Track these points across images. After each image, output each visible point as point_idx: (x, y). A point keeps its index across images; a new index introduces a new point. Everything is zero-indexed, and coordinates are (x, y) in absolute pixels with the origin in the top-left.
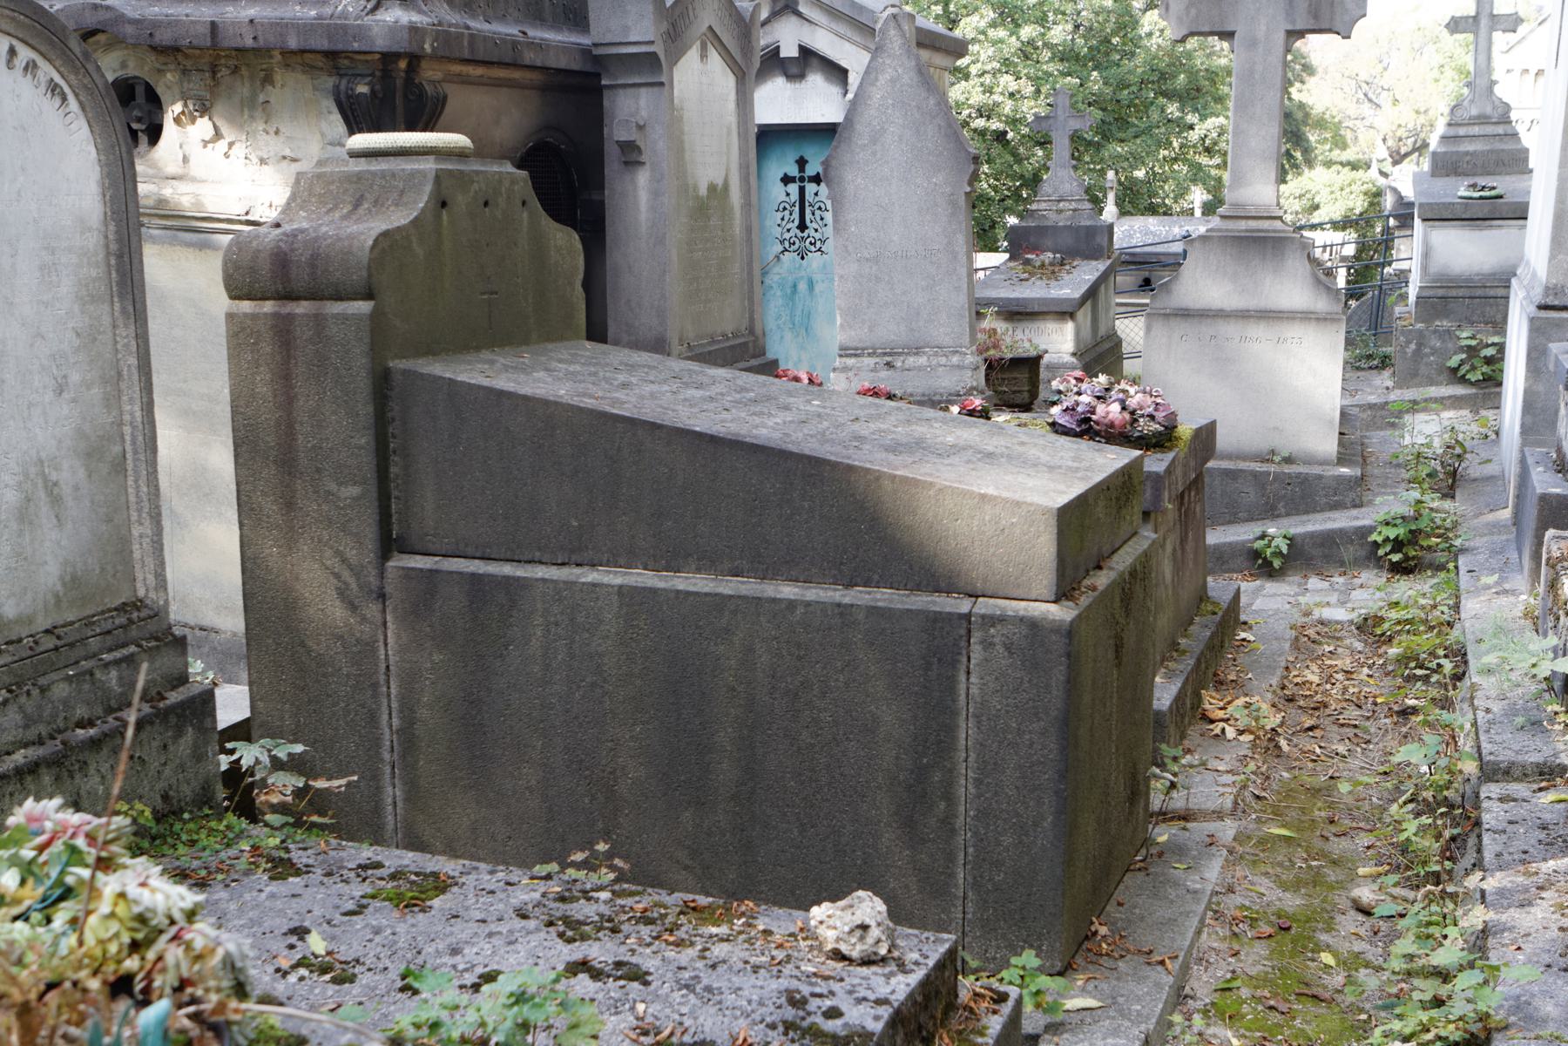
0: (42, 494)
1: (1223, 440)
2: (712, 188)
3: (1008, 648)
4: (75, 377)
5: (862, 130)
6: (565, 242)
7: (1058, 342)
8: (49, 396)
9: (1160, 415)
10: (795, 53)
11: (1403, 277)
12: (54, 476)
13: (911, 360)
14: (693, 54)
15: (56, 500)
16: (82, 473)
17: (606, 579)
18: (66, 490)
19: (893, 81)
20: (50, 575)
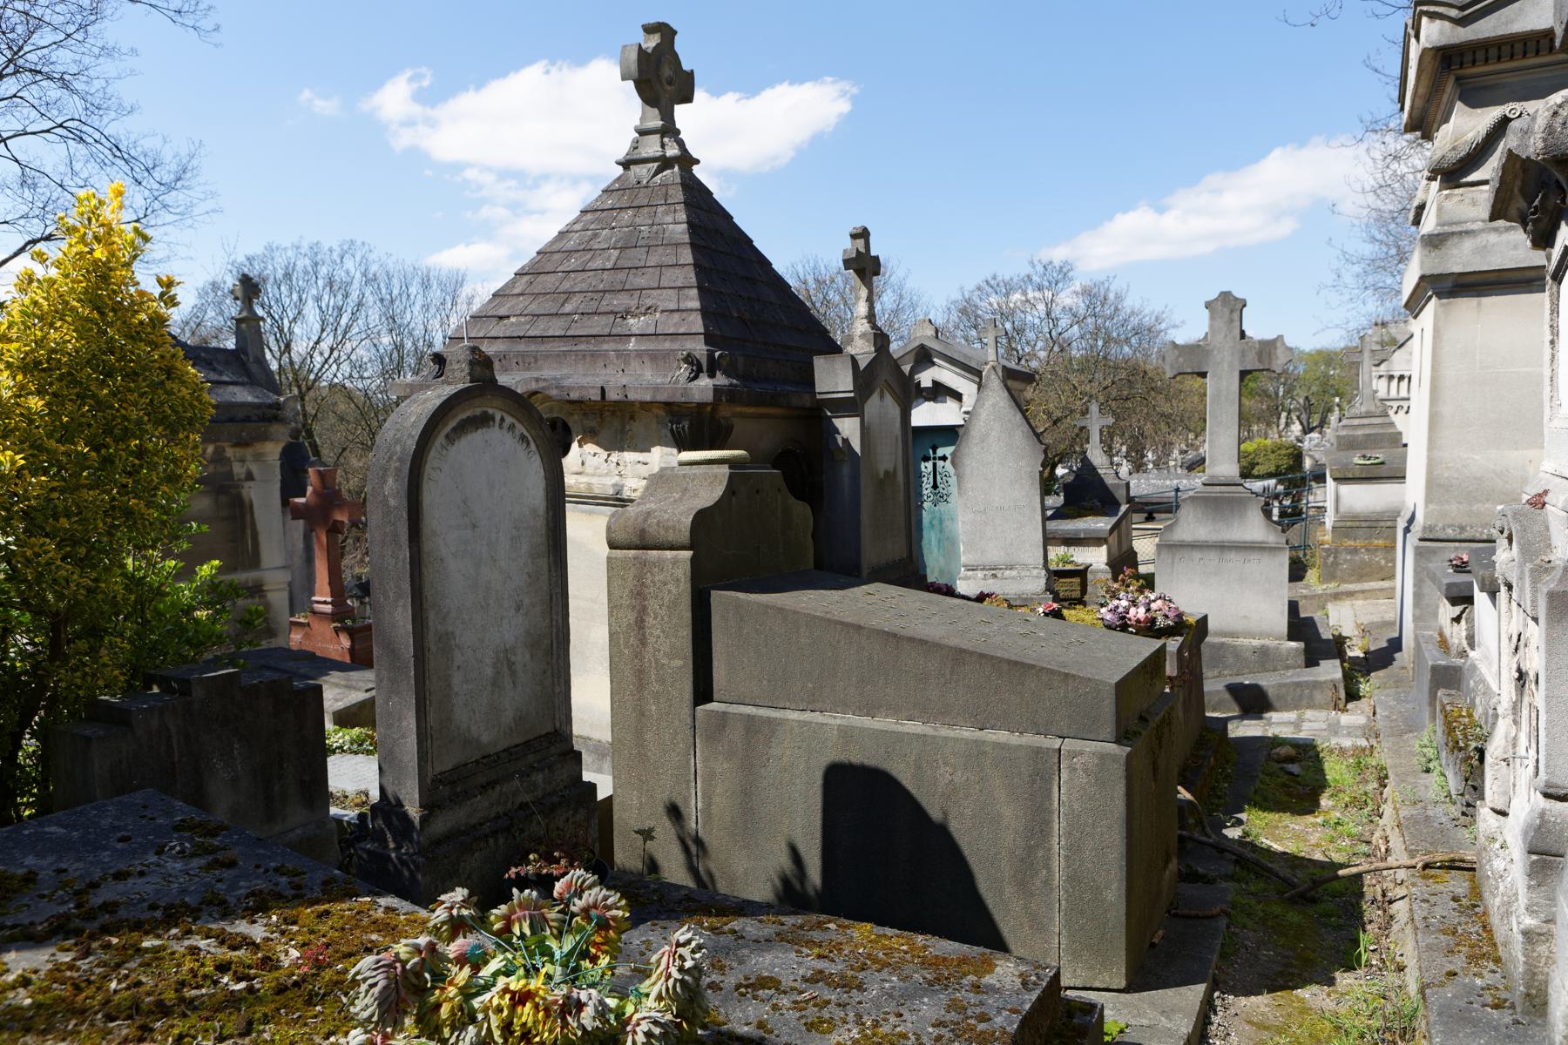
0: (505, 669)
1: (1211, 625)
2: (887, 473)
3: (1085, 771)
4: (526, 601)
5: (976, 431)
6: (801, 510)
7: (1096, 558)
8: (512, 612)
9: (1171, 615)
10: (930, 384)
11: (1322, 510)
12: (513, 658)
13: (1007, 572)
14: (875, 397)
15: (513, 673)
16: (528, 656)
17: (832, 721)
18: (519, 667)
19: (994, 405)
20: (508, 716)
